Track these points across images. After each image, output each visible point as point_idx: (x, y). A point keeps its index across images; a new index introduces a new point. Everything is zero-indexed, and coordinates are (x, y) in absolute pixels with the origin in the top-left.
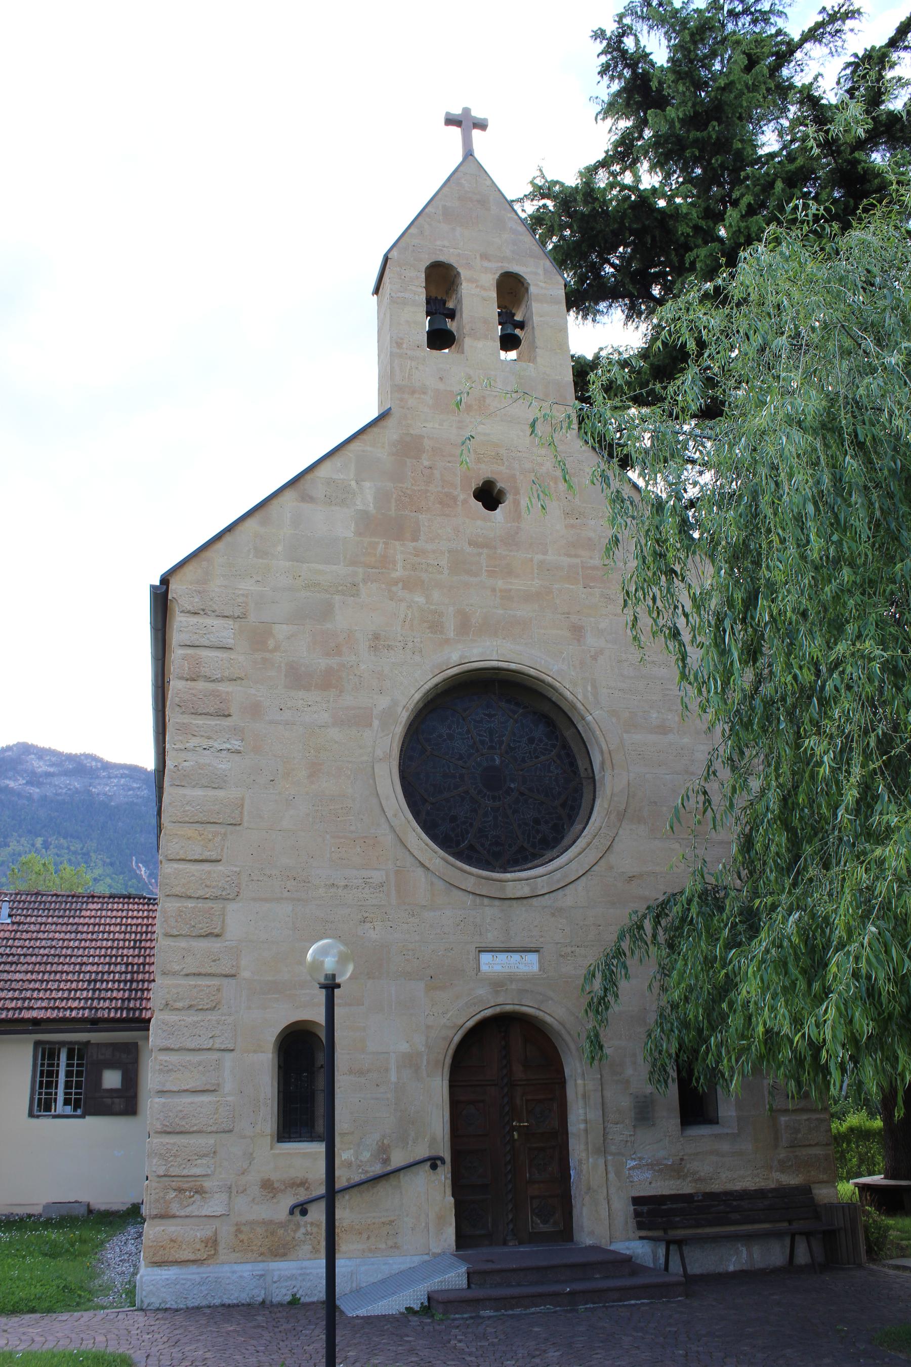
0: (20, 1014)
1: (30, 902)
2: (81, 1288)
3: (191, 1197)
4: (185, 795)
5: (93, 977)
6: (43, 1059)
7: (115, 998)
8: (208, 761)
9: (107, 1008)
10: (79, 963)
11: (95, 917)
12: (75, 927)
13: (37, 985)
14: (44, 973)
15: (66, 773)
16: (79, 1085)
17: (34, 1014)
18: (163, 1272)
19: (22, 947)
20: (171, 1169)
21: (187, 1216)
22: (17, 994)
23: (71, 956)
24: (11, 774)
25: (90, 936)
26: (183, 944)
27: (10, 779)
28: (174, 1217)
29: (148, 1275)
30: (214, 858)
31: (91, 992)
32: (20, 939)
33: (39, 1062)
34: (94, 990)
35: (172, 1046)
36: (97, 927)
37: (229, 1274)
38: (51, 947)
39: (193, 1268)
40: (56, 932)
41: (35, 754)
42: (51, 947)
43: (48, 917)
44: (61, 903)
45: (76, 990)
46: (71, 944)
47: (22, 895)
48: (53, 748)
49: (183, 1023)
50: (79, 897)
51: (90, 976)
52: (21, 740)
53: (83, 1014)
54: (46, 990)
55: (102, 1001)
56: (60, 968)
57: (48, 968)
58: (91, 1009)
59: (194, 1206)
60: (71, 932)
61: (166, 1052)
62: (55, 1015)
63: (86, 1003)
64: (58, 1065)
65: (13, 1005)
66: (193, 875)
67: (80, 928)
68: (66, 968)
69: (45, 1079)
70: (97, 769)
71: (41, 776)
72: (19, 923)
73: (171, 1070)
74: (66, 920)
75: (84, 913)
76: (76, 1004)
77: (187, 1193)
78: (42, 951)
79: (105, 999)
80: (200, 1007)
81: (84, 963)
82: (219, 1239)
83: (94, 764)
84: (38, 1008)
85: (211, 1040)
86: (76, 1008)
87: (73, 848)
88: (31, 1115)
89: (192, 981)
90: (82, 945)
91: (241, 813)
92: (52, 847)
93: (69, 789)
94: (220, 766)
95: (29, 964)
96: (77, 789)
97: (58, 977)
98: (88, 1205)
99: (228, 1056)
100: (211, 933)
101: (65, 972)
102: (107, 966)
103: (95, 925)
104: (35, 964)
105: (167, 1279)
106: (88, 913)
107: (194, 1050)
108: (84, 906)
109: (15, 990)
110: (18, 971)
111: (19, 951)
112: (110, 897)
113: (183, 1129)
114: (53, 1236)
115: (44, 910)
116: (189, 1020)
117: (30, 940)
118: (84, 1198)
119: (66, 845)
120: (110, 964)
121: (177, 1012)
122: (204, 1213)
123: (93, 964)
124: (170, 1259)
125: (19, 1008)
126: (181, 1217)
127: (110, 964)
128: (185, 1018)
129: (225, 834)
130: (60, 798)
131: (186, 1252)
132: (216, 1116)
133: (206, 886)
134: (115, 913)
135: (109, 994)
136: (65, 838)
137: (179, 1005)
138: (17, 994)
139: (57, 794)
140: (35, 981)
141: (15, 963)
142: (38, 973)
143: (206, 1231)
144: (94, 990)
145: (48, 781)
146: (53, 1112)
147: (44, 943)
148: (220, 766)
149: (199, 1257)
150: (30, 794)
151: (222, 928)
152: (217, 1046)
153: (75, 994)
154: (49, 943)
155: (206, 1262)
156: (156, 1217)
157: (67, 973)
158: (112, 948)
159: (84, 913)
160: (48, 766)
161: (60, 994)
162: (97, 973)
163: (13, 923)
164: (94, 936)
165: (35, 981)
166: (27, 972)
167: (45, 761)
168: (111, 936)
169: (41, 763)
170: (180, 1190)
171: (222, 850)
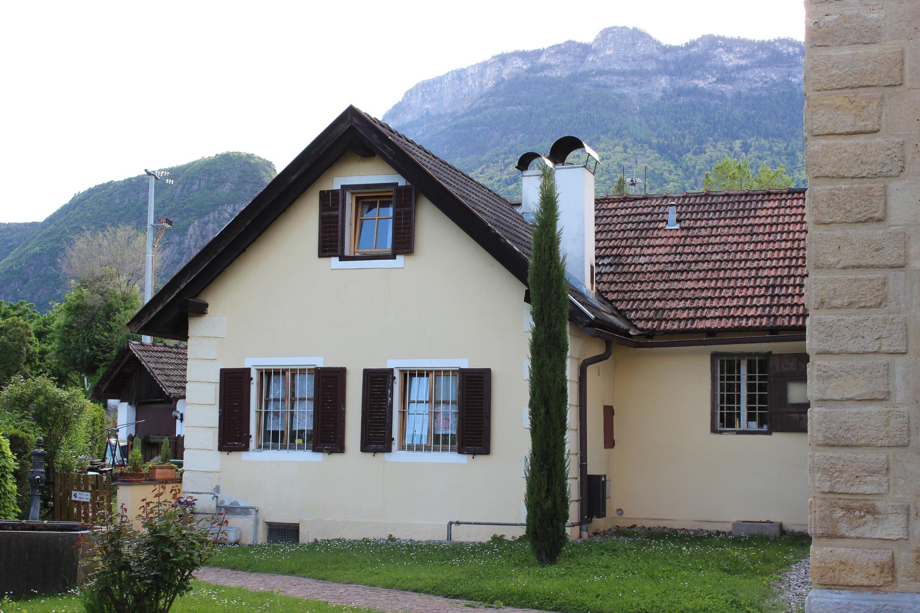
0: (692, 324)
1: (699, 205)
2: (751, 605)
3: (861, 517)
4: (829, 57)
5: (771, 282)
6: (722, 372)
7: (796, 304)
8: (856, 12)
9: (788, 315)
10: (755, 268)
11: (772, 217)
12: (750, 228)
13: (710, 294)
14: (717, 280)
15: (761, 64)
16: (762, 400)
17: (708, 324)
18: (834, 595)
19: (693, 254)
20: (837, 486)
21: (857, 538)
22: (688, 304)
23: (746, 261)
24: (699, 72)
25: (766, 238)
26: (838, 232)
27: (698, 78)
28: (843, 537)
29: (817, 597)
30: (869, 128)
31: (769, 298)
32: (690, 245)
33: (719, 375)
34: (773, 296)
35: (831, 350)
36: (774, 227)
37: (910, 605)
38: (724, 252)
39: (868, 595)
40: (728, 236)
41: (723, 47)
42: (724, 252)
43: (719, 219)
44: (733, 203)
45: (752, 297)
46: (746, 247)
47: (690, 198)
48: (742, 36)
49: (842, 323)
50: (752, 195)
51: (768, 281)
52: (706, 33)
53: (761, 323)
54: (719, 298)
55: (781, 308)
56: (734, 274)
57: (722, 274)
58: (769, 317)
59: (866, 528)
60: (745, 235)
61: (823, 356)
62: (729, 325)
63: (763, 310)
64: (739, 378)
65: (685, 315)
66: (846, 151)
67: (755, 230)
68: (740, 273)
69: (725, 393)
70: (796, 55)
71: (732, 71)
72: (688, 229)
73: (831, 376)
74: (739, 221)
75: (759, 213)
76: (752, 312)
77: (857, 513)
78: (714, 257)
79: (784, 306)
80: (862, 305)
81: (761, 267)
82: (897, 563)
83: (791, 49)
84: (711, 318)
85: (878, 342)
86: (752, 316)
87: (775, 149)
88: (714, 430)
89: (851, 275)
90: (758, 248)
91: (902, 70)
92: (752, 149)
93: (766, 82)
94: (871, 16)
95: (700, 271)
96: (774, 81)
97: (732, 283)
98: (781, 525)
99: (899, 360)
100: (871, 218)
101: (741, 278)
102: (787, 269)
103: (771, 225)
104: (707, 271)
105: (839, 603)
106: (764, 213)
107: (857, 353)
108: (759, 205)
109: (686, 299)
110: (690, 280)
111: (690, 258)
112: (788, 194)
113: (849, 442)
114: (736, 553)
115: (715, 212)
116: (851, 319)
117: (701, 245)
118: (776, 518)
119: (767, 146)
120: (789, 267)
121: (836, 311)
122: (877, 535)
123: (771, 268)
124: (841, 582)
125: (691, 318)
126: (851, 538)
127: (789, 267)
128: (845, 317)
129: (882, 98)
130: (756, 93)
131: (859, 576)
132: (887, 428)
133: (862, 162)
134: (794, 211)
135: (789, 300)
136: (765, 138)
137: (837, 302)
138: (688, 304)
139: (752, 90)
140: (708, 289)
141: (685, 270)
142: (711, 280)
143: (883, 556)
144: (773, 296)
145: (741, 75)
146: (737, 428)
147: (716, 248)
148: (871, 16)
149: (874, 583)
150: (722, 92)
151: (885, 211)
152: (884, 348)
153: (751, 302)
154: (722, 248)
155: (882, 589)
156: (822, 536)
157: (743, 279)
158: (792, 249)
159: (759, 213)
160: (738, 58)
161: (735, 302)
162: (776, 278)
163: (682, 229)
164: (772, 238)
165: (708, 289)
166: (698, 280)
167: (735, 53)
168: (791, 236)
169: (731, 56)
170: (848, 509)
171: (879, 118)
